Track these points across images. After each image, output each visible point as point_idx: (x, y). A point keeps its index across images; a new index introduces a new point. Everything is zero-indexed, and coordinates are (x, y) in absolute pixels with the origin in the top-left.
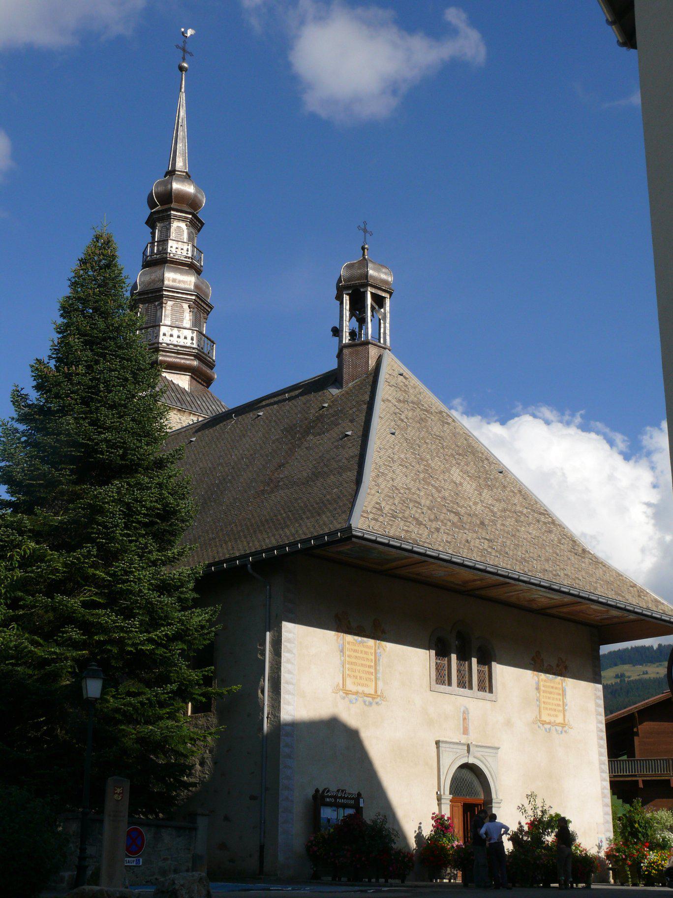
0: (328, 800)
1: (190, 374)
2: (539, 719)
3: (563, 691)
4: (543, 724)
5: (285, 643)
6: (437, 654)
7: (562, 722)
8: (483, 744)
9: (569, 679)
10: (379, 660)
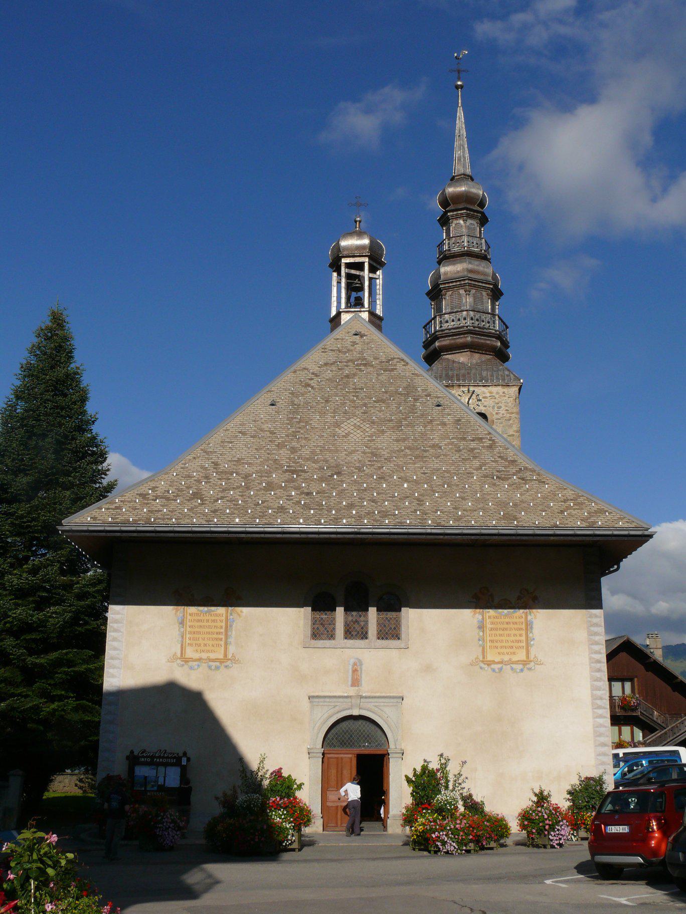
0: (143, 760)
1: (468, 350)
2: (481, 659)
3: (527, 625)
4: (488, 665)
5: (111, 624)
6: (313, 610)
7: (524, 658)
8: (383, 694)
9: (539, 610)
10: (231, 626)
